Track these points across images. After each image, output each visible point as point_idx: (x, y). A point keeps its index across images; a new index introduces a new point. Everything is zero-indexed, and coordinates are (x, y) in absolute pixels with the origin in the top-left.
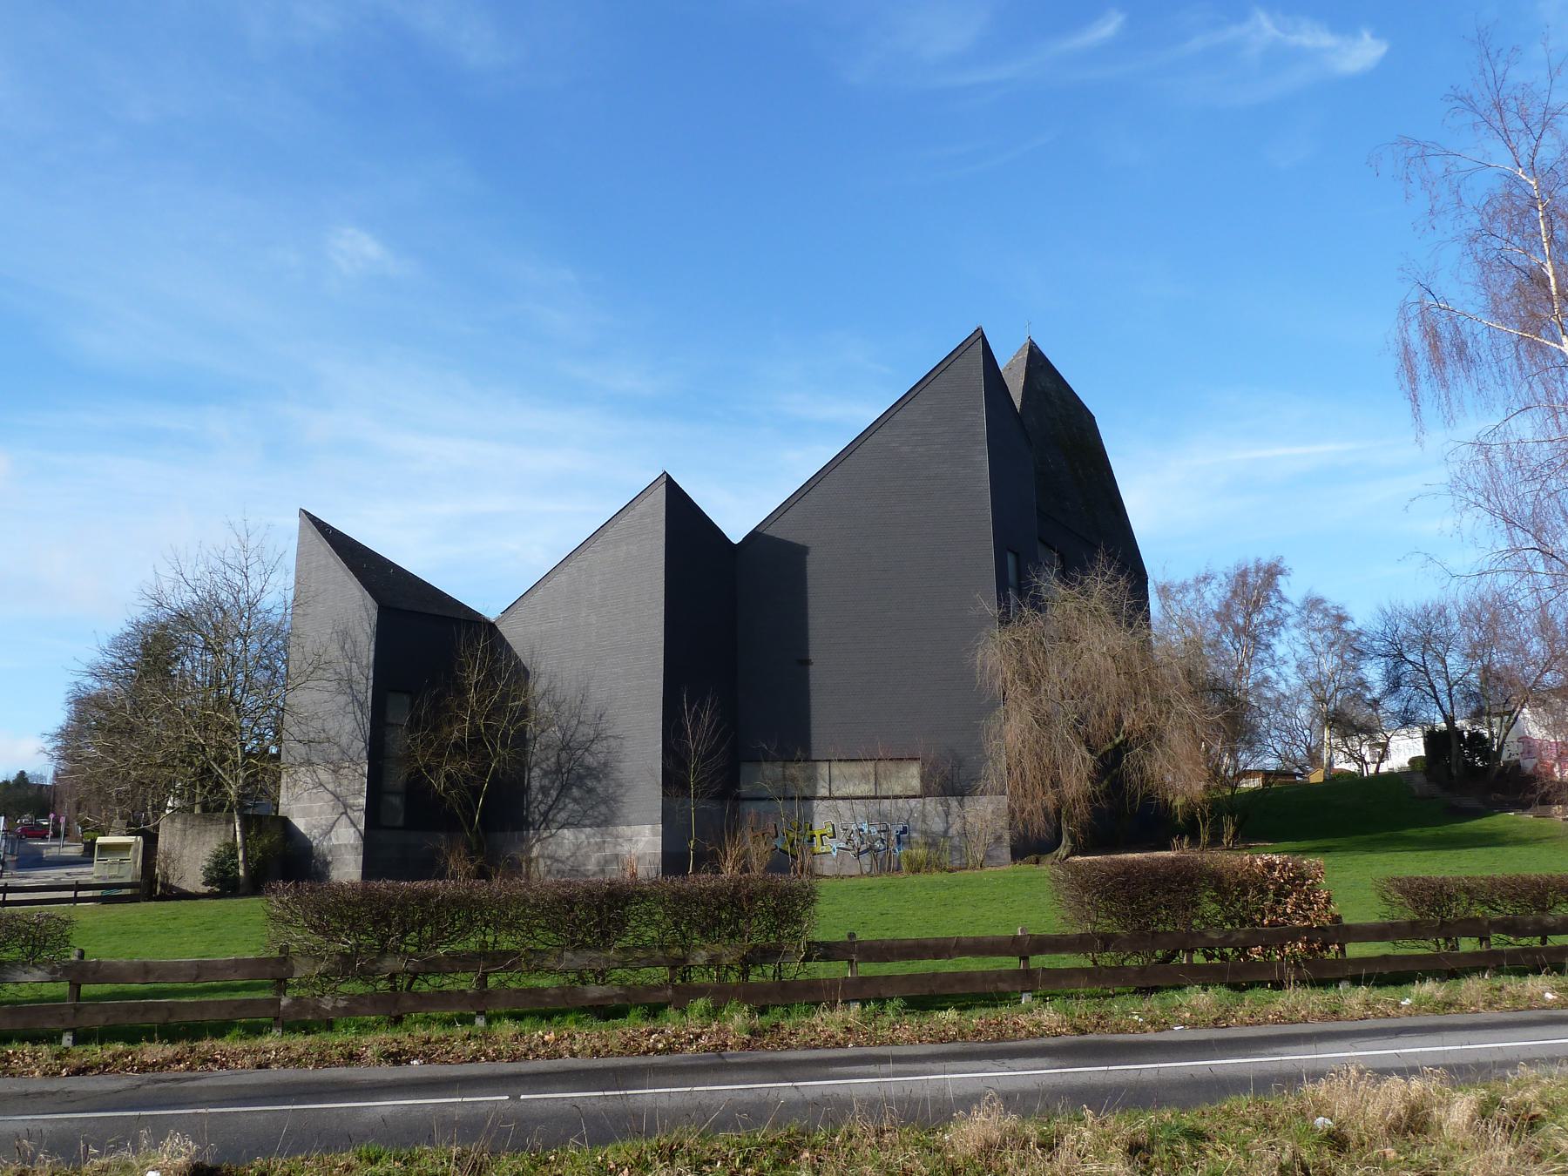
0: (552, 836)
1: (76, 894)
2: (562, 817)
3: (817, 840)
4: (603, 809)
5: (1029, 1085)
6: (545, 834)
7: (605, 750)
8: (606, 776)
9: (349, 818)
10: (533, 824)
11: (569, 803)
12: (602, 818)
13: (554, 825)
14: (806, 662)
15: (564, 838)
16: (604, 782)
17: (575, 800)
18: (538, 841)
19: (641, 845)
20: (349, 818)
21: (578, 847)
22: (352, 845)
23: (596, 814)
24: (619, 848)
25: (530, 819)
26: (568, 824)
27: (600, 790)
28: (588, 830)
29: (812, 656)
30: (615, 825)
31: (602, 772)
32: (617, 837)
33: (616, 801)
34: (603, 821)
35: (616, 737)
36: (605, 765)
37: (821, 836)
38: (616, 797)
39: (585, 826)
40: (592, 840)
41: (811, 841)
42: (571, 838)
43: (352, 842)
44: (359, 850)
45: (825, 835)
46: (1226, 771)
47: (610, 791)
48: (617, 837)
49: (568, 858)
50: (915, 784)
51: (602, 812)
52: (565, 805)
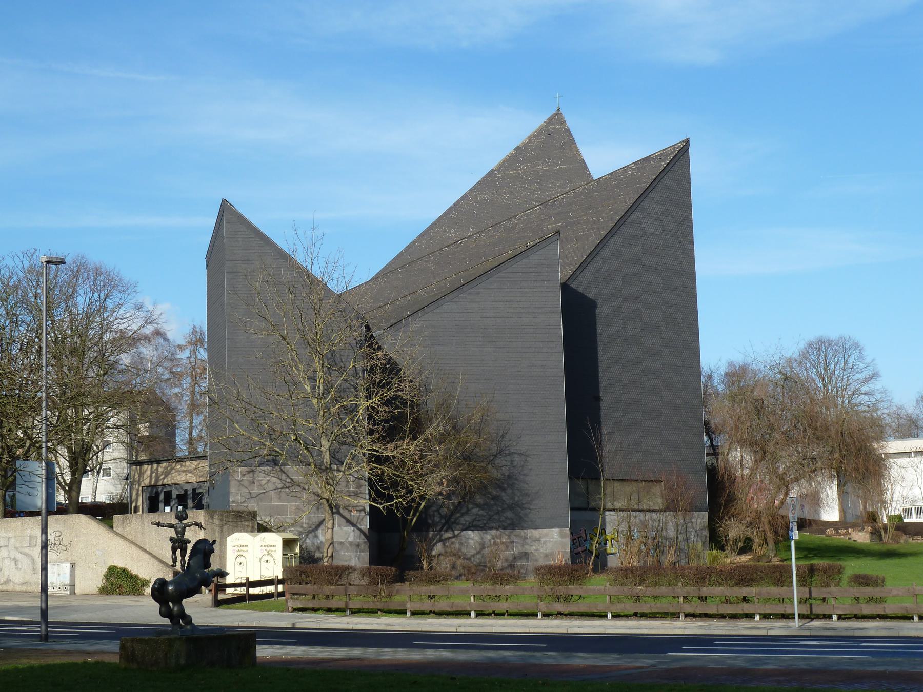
0: (455, 536)
1: (248, 591)
2: (467, 519)
3: (609, 543)
4: (509, 514)
5: (802, 665)
6: (448, 535)
7: (509, 464)
8: (512, 486)
9: (344, 517)
10: (434, 525)
11: (473, 508)
12: (508, 522)
13: (458, 527)
14: (598, 399)
15: (468, 538)
16: (509, 491)
17: (478, 506)
18: (440, 540)
19: (549, 545)
20: (344, 517)
21: (483, 546)
22: (351, 544)
23: (502, 519)
24: (527, 547)
25: (430, 521)
26: (473, 526)
27: (505, 497)
28: (493, 532)
29: (602, 394)
30: (523, 528)
31: (509, 481)
32: (526, 538)
33: (523, 508)
34: (510, 524)
35: (520, 454)
36: (509, 477)
37: (611, 539)
38: (523, 504)
39: (491, 529)
40: (498, 540)
41: (606, 544)
42: (476, 538)
43: (350, 539)
44: (362, 547)
45: (614, 539)
46: (326, 463)
47: (517, 499)
48: (526, 538)
49: (473, 556)
50: (659, 502)
51: (509, 517)
52: (468, 510)
